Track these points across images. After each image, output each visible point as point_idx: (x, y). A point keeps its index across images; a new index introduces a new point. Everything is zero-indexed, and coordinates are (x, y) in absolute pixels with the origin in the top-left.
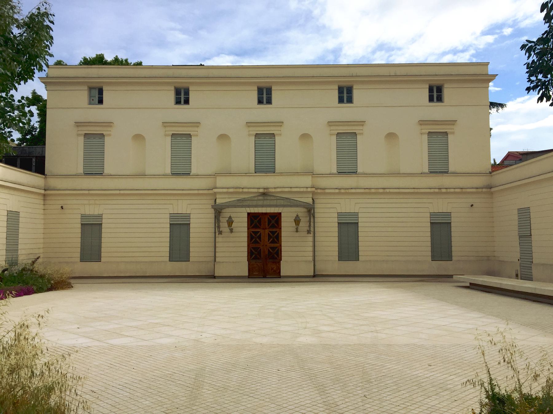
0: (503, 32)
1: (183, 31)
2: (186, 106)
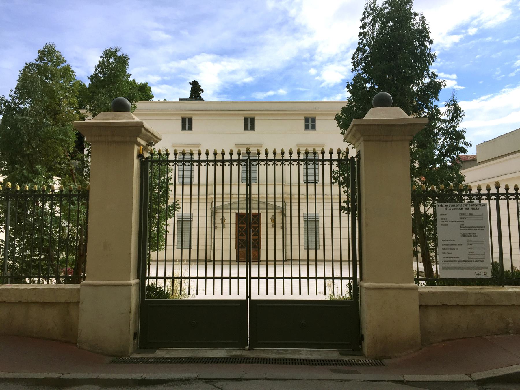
0: (468, 32)
1: (167, 32)
2: (190, 132)
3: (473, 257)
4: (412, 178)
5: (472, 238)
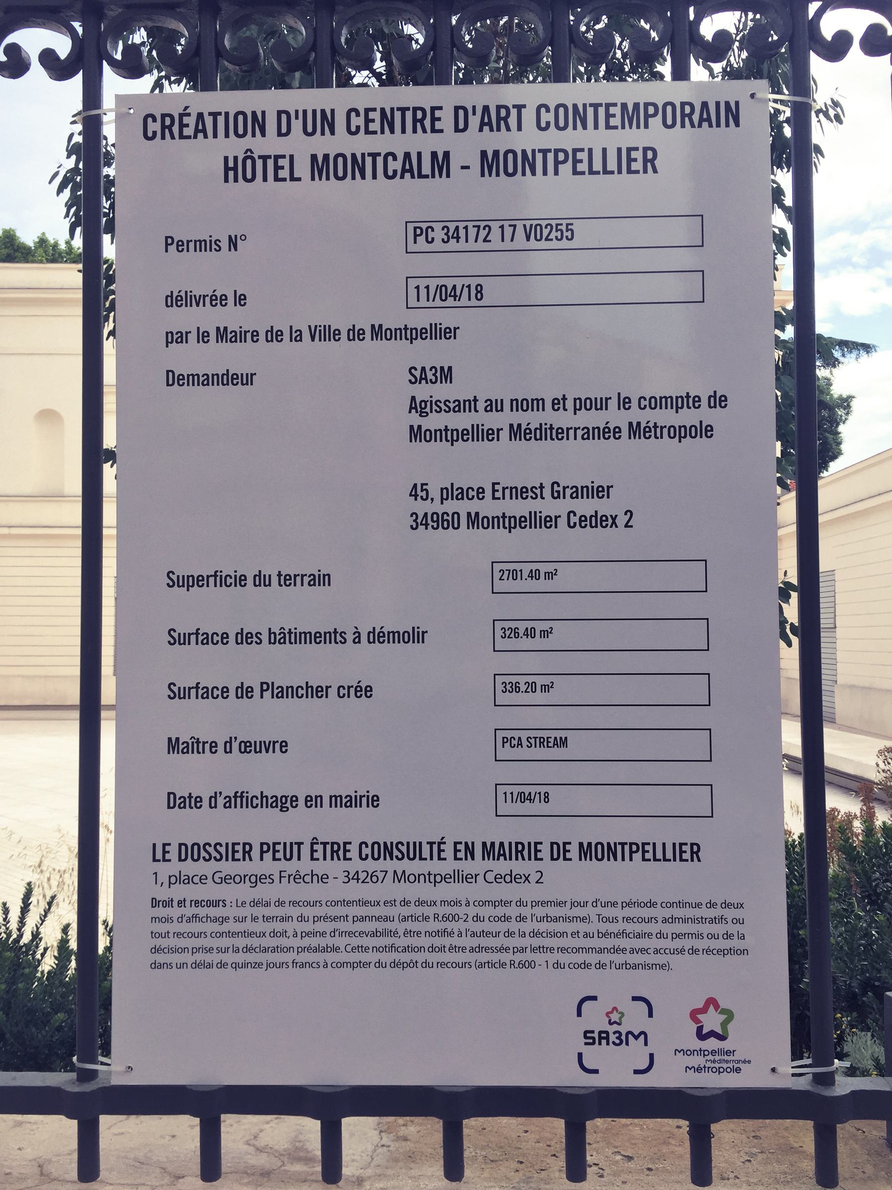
3: (560, 801)
4: (353, 86)
5: (562, 542)
